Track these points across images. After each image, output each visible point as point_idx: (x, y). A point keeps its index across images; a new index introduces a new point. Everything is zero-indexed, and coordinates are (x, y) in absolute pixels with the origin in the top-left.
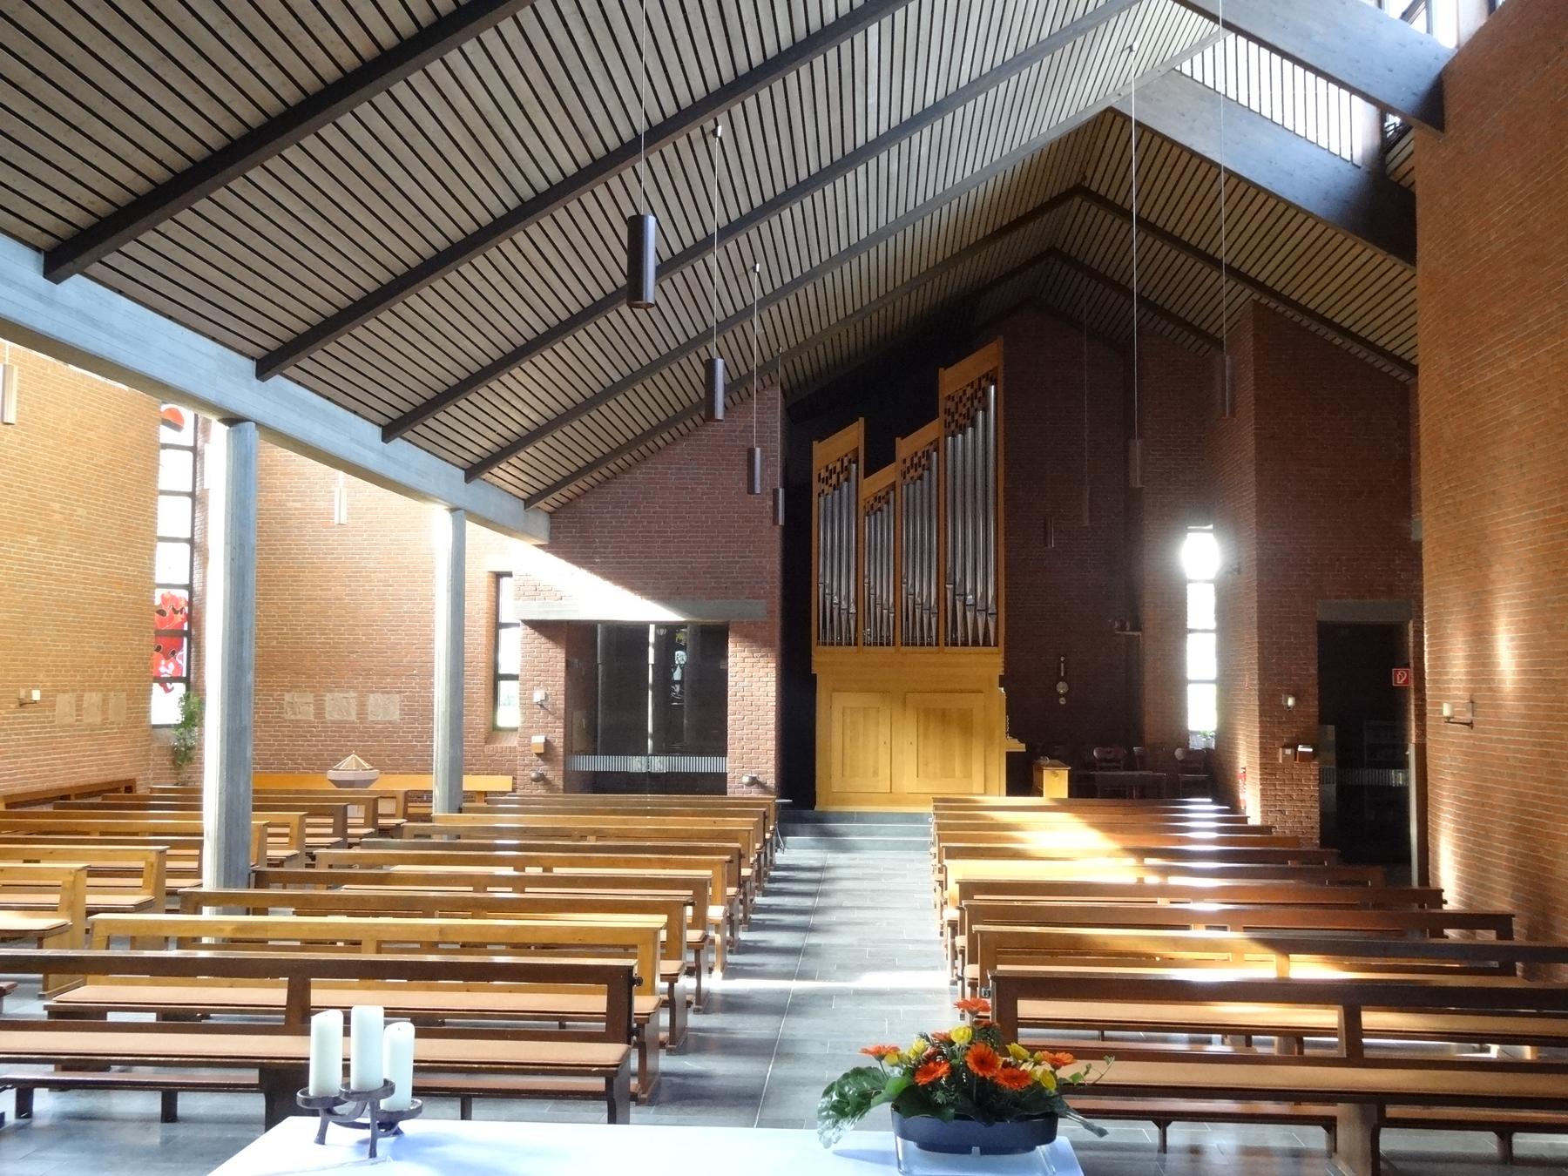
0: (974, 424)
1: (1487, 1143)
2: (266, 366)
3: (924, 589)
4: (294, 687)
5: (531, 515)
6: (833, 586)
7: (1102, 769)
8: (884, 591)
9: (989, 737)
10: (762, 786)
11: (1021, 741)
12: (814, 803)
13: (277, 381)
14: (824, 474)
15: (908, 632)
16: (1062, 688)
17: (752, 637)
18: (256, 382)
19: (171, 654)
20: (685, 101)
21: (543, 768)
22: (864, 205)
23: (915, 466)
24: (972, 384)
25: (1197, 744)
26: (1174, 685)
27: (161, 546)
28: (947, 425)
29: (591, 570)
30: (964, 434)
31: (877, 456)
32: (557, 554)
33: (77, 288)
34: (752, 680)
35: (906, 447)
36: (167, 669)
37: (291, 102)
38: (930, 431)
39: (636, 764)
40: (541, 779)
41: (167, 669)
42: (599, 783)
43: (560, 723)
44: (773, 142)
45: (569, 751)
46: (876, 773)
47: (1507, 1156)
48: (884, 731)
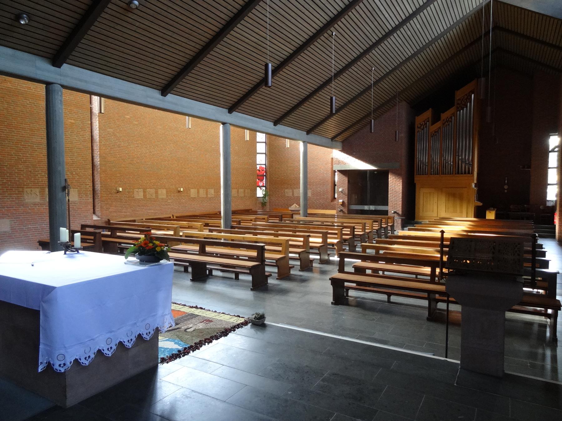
0: (467, 107)
1: (384, 297)
2: (231, 110)
3: (449, 158)
4: (287, 188)
5: (334, 142)
6: (421, 157)
7: (513, 212)
8: (437, 159)
9: (469, 202)
10: (398, 214)
11: (481, 202)
12: (414, 219)
13: (234, 113)
14: (419, 126)
15: (442, 171)
16: (506, 187)
17: (397, 173)
18: (229, 114)
19: (262, 180)
20: (404, 17)
21: (342, 208)
22: (401, 46)
23: (447, 121)
24: (466, 95)
25: (549, 204)
26: (543, 184)
27: (258, 155)
28: (457, 108)
29: (353, 156)
30: (463, 110)
31: (436, 119)
32: (344, 152)
33: (170, 97)
34: (395, 185)
35: (444, 116)
36: (261, 184)
37: (200, 48)
38: (452, 110)
39: (366, 208)
40: (341, 211)
41: (261, 184)
42: (350, 212)
43: (346, 197)
44: (356, 34)
45: (350, 203)
46: (433, 211)
47: (389, 301)
48: (436, 199)
